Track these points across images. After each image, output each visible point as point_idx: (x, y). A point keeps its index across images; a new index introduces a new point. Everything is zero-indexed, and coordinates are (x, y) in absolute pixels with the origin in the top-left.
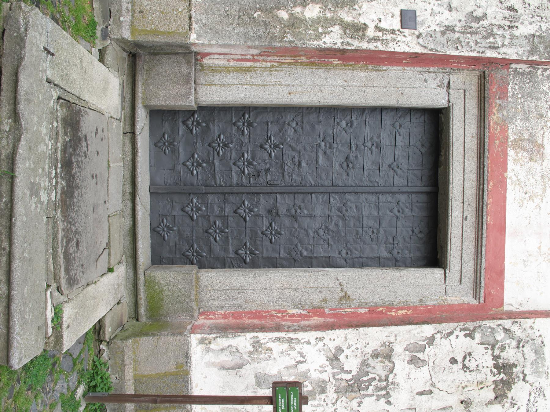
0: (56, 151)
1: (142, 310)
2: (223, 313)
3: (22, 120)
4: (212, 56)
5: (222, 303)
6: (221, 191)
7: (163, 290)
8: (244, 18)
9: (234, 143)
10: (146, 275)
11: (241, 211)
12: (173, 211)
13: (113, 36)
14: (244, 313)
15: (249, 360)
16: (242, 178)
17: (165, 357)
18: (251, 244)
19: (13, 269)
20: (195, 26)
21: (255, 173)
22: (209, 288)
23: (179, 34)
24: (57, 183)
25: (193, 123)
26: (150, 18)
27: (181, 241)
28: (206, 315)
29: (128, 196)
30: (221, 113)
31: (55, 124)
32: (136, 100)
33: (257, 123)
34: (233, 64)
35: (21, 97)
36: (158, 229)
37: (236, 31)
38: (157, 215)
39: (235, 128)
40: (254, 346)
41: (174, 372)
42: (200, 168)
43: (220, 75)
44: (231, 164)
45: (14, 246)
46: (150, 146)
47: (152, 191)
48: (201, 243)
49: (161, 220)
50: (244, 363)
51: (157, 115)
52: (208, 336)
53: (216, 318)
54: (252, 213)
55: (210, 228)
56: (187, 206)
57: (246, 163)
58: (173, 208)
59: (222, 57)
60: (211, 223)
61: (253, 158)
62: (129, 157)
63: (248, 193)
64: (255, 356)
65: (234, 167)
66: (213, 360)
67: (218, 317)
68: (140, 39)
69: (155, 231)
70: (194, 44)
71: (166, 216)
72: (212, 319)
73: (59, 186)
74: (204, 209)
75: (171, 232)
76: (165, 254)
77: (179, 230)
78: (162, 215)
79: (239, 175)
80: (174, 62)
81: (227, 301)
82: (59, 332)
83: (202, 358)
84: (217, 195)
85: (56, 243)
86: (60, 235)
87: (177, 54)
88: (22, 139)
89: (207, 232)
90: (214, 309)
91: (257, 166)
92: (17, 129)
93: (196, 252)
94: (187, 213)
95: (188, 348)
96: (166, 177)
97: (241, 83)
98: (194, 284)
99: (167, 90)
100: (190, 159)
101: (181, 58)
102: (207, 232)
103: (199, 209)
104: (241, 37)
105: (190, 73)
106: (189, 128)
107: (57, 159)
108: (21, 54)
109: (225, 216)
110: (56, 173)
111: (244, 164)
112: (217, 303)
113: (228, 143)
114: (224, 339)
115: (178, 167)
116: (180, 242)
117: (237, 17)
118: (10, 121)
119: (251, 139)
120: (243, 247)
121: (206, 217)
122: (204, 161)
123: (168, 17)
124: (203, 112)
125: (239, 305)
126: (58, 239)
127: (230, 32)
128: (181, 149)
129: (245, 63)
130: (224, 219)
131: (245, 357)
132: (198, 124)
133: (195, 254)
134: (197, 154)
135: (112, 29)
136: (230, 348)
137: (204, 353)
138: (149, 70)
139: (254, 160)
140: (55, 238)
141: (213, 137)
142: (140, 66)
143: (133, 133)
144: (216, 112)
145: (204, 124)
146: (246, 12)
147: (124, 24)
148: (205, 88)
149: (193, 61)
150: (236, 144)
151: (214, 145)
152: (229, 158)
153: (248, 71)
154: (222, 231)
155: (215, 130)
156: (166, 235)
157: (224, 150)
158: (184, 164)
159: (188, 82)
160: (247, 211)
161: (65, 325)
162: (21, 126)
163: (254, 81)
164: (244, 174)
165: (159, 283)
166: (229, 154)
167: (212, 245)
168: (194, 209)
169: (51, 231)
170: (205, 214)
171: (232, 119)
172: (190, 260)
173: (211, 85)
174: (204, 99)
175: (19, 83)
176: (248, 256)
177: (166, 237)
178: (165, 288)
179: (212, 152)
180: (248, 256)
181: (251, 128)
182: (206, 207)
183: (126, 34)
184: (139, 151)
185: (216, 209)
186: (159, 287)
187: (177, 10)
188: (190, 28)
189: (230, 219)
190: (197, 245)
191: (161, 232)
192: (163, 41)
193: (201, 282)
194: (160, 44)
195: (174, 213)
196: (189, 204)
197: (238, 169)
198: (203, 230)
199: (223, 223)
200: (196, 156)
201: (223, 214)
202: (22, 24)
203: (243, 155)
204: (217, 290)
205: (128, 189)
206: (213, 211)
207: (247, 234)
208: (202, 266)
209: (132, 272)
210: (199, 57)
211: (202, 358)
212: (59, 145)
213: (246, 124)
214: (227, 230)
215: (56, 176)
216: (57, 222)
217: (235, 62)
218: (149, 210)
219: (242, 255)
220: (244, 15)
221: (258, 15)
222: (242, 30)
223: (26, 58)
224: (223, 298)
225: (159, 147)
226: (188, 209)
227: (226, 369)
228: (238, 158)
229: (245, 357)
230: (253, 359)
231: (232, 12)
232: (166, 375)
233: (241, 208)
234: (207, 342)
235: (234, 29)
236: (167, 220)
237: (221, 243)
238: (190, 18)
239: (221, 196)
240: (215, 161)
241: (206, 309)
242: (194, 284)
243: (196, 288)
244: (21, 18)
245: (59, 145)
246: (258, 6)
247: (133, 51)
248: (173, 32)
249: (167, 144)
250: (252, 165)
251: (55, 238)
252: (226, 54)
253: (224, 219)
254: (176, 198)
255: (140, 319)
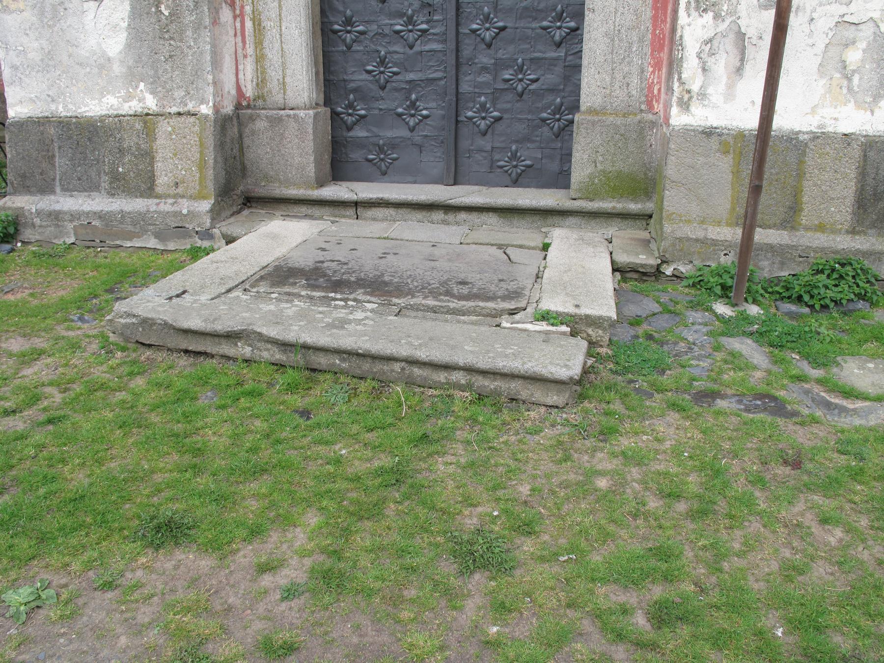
0: (311, 298)
1: (634, 207)
2: (651, 69)
3: (236, 329)
4: (242, 82)
5: (635, 70)
6: (454, 69)
7: (604, 171)
8: (172, 31)
9: (379, 48)
10: (576, 197)
11: (488, 35)
12: (485, 149)
13: (208, 224)
14: (655, 30)
15: (731, 20)
16: (434, 34)
17: (704, 172)
18: (544, 19)
19: (427, 360)
20: (190, 106)
21: (426, 11)
22: (608, 92)
23: (203, 130)
24: (355, 300)
25: (350, 115)
26: (184, 172)
27: (535, 138)
28: (652, 100)
29: (451, 217)
30: (332, 69)
31: (273, 296)
32: (309, 198)
33: (346, 8)
34: (250, 50)
35: (209, 327)
36: (514, 175)
37: (192, 44)
38: (491, 175)
39: (356, 47)
40: (705, 11)
41: (733, 158)
42: (418, 103)
43: (269, 70)
44: (411, 52)
45: (395, 354)
46: (386, 182)
47: (452, 182)
48: (540, 105)
49: (499, 170)
50: (737, 29)
51: (338, 167)
52: (676, 94)
53: (659, 83)
54: (492, 16)
55: (515, 89)
56: (478, 126)
57: (410, 27)
58: (481, 150)
59: (241, 67)
60: (506, 87)
61: (402, 15)
62: (391, 211)
63: (458, 24)
64: (725, 8)
65: (417, 48)
66: (722, 87)
67: (658, 78)
68: (211, 186)
69: (517, 180)
70: (216, 110)
71: (492, 162)
72: (659, 90)
73: (359, 297)
74: (483, 98)
75: (519, 154)
76: (555, 166)
77: (517, 141)
78: (491, 167)
79: (429, 39)
80: (253, 141)
81: (632, 61)
82: (581, 319)
83: (715, 107)
84: (461, 76)
85: (442, 309)
86: (431, 302)
87: (241, 136)
88: (259, 330)
89: (521, 95)
90: (643, 85)
91: (413, 8)
92: (248, 336)
93: (554, 114)
94: (489, 127)
95: (694, 131)
96: (432, 159)
97: (278, 36)
98: (596, 118)
99: (293, 151)
100: (404, 120)
101: (247, 130)
102: (521, 95)
103: (483, 107)
104: (199, 35)
105: (267, 117)
106: (358, 121)
107: (323, 297)
108: (160, 324)
109: (495, 64)
110: (341, 300)
111: (411, 31)
112: (635, 81)
113: (380, 57)
114: (685, 65)
115: (417, 139)
116: (536, 141)
117: (172, 42)
118: (239, 344)
119: (372, 18)
120: (549, 33)
121: (495, 96)
122: (408, 98)
123: (180, 147)
124: (332, 97)
125: (641, 40)
126: (436, 306)
127: (194, 53)
128: (389, 134)
129: (247, 30)
130: (500, 65)
131: (723, 27)
132: (351, 106)
133: (558, 116)
134: (396, 108)
135: (199, 225)
136: (702, 55)
137: (706, 103)
138: (266, 177)
139: (405, 14)
140: (434, 310)
141: (370, 81)
142: (261, 192)
143: (356, 204)
144: (332, 77)
145: (352, 96)
146: (164, 29)
147: (192, 208)
148: (289, 93)
149: (250, 111)
150: (381, 45)
151: (382, 81)
152: (402, 56)
153: (259, 25)
154: (521, 69)
155: (359, 78)
156: (524, 163)
157: (390, 65)
158: (412, 130)
159: (280, 119)
160: (487, 25)
161: (571, 310)
162: (243, 330)
163: (273, 14)
164: (428, 30)
165: (591, 177)
166: (396, 56)
167: (544, 87)
168: (484, 115)
169: (420, 314)
170: (491, 97)
171: (343, 52)
172: (567, 126)
173: (284, 83)
174: (306, 94)
175: (192, 328)
176: (564, 25)
177: (528, 162)
178: (600, 167)
179: (394, 84)
180: (564, 25)
181: (354, 19)
182: (480, 95)
183: (205, 206)
184: (380, 196)
185: (484, 79)
186: (598, 177)
187: (170, 134)
188: (193, 115)
189: (500, 54)
190: (542, 112)
191: (519, 171)
192: (212, 153)
193: (596, 106)
194: (219, 159)
195: (489, 148)
196: (474, 123)
197: (419, 41)
198: (517, 101)
199: (507, 67)
200: (400, 110)
201: (492, 67)
202: (128, 320)
203: (397, 32)
204: (613, 78)
205: (439, 215)
206: (486, 84)
207: (527, 25)
208: (575, 107)
209: (571, 218)
210: (244, 103)
211: (715, 107)
212: (303, 293)
213: (349, 28)
214: (520, 60)
215: (345, 300)
216: (411, 305)
217: (247, 46)
218: (481, 187)
219: (564, 34)
220: (168, 31)
221: (167, 7)
222: (189, 33)
223: (165, 318)
224: (626, 69)
225: (388, 168)
226: (483, 124)
227: (742, 64)
228: (402, 40)
229: (723, 27)
230: (730, 13)
231: (165, 50)
232: (738, 172)
233: (482, 36)
234: (686, 97)
235: (189, 47)
236: (499, 161)
237: (540, 72)
238: (179, 114)
239: (464, 68)
240: (408, 78)
241: (643, 99)
242: (596, 118)
243: (605, 114)
244: (122, 321)
245: (303, 293)
246: (153, 9)
247: (241, 201)
248: (200, 141)
249: (382, 156)
250: (412, 17)
251: (434, 310)
252: (237, 61)
253: (500, 65)
254: (464, 144)
255: (649, 212)
